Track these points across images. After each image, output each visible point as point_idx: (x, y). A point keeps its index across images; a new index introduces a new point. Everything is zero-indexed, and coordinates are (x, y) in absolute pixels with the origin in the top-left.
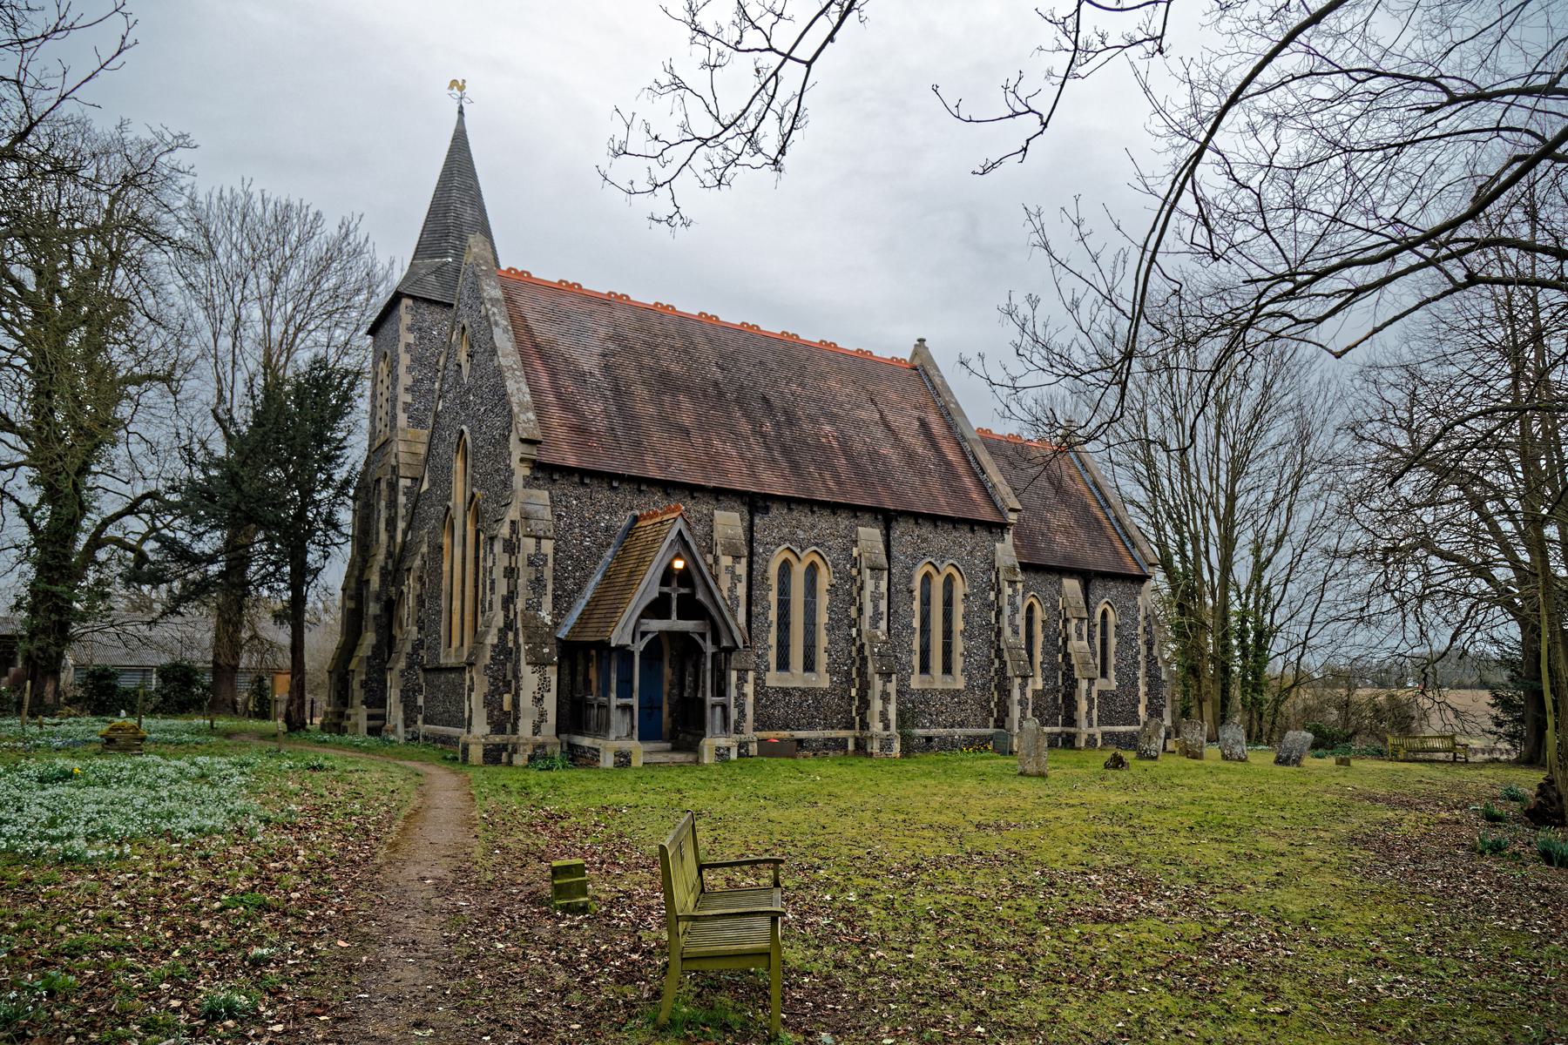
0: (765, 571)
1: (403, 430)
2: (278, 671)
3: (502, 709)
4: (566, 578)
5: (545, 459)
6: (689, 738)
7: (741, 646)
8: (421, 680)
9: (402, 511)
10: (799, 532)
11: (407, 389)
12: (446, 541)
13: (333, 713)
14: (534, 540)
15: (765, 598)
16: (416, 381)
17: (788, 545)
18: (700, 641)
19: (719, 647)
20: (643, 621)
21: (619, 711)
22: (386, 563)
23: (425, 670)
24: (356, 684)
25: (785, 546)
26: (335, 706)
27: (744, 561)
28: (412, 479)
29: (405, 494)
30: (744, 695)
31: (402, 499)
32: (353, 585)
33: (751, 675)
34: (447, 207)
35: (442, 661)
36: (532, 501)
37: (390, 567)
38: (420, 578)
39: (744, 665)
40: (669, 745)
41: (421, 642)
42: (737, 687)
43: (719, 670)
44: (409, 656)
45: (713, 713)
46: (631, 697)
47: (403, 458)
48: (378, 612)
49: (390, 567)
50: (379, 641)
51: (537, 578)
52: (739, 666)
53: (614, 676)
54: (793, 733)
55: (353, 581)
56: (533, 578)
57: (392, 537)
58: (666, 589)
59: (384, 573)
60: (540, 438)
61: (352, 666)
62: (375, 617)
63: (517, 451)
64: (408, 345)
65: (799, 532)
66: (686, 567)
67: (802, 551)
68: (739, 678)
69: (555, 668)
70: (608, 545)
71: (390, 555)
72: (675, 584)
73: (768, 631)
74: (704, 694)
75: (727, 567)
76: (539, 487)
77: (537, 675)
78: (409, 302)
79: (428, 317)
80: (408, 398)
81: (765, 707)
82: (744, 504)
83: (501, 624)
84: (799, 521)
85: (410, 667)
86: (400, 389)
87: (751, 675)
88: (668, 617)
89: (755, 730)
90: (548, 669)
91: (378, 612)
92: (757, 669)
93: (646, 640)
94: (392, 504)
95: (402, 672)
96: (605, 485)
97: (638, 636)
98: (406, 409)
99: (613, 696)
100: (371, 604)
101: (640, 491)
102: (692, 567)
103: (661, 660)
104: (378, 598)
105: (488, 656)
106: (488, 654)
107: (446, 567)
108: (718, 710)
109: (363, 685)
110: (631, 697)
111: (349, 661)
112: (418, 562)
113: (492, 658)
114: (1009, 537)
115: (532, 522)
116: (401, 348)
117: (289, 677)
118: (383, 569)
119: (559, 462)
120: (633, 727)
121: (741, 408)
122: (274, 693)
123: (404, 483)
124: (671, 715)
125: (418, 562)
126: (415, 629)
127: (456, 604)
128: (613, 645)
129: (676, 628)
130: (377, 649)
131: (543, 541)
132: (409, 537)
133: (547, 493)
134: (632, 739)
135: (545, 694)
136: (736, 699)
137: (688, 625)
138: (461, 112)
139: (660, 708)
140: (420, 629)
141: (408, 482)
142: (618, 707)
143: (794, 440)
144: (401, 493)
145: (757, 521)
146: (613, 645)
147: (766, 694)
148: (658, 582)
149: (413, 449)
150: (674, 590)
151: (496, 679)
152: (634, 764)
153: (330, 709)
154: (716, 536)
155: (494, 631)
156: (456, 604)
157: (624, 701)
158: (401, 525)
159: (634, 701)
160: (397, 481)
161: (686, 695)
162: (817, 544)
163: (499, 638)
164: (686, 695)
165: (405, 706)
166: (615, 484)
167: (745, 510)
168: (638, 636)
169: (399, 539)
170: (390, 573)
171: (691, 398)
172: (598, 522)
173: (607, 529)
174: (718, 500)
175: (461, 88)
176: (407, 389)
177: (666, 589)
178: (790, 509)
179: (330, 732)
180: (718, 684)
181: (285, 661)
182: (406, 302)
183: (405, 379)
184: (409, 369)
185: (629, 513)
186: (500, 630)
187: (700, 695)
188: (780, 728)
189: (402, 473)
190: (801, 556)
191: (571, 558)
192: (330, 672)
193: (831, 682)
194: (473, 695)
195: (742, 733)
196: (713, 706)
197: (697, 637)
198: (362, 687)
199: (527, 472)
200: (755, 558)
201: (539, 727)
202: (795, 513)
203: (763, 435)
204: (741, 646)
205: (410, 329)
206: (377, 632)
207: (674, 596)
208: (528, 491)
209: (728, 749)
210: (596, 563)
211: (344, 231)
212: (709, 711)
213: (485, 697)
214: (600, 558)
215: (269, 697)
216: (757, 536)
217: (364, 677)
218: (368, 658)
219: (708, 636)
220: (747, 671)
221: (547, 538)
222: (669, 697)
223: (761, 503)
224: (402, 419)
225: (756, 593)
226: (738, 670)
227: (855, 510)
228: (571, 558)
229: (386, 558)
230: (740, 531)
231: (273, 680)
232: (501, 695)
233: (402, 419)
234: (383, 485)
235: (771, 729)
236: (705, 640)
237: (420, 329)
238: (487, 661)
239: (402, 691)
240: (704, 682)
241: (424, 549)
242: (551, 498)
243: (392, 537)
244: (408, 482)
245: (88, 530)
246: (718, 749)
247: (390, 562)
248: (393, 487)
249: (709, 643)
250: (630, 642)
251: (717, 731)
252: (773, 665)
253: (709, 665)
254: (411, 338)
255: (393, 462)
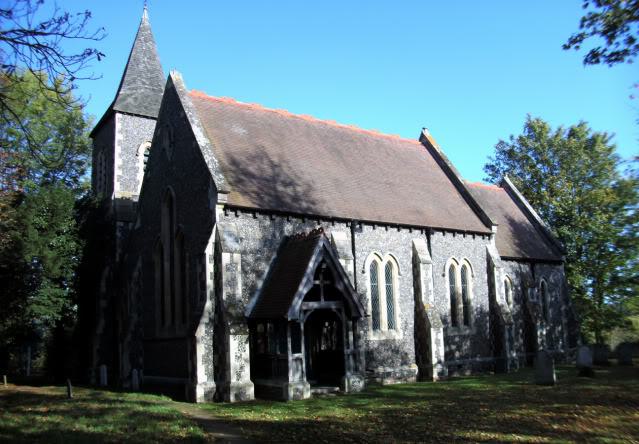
12: (156, 258)
53: (289, 340)
64: (120, 141)
79: (131, 124)
99: (290, 352)
107: (157, 275)
114: (493, 241)
127: (168, 298)
137: (333, 306)
140: (139, 315)
145: (356, 237)
156: (168, 298)
157: (296, 355)
159: (301, 355)
162: (390, 250)
179: (504, 419)
193: (404, 335)
227: (410, 228)
245: (569, 141)
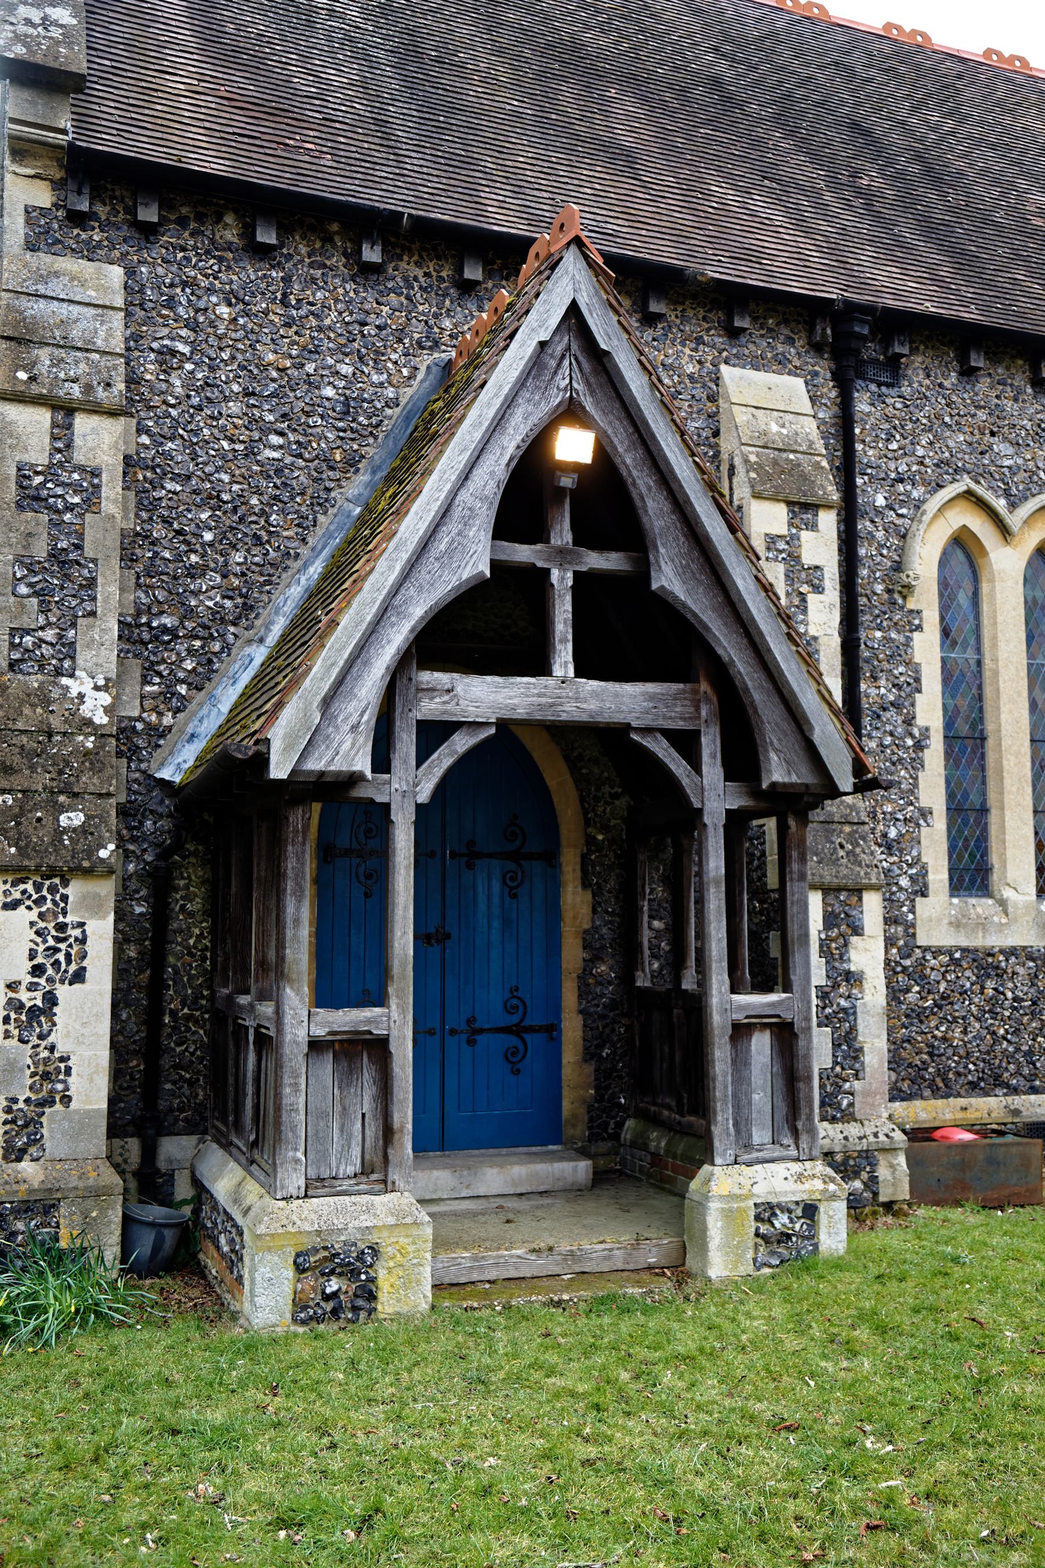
0: (898, 567)
4: (194, 573)
5: (107, 143)
6: (658, 1140)
7: (845, 781)
10: (1000, 447)
14: (43, 417)
15: (901, 653)
17: (965, 483)
18: (678, 766)
19: (756, 792)
20: (426, 677)
21: (326, 1067)
25: (959, 487)
27: (828, 521)
30: (853, 979)
33: (872, 906)
36: (55, 288)
39: (844, 872)
40: (581, 1169)
42: (825, 950)
43: (759, 892)
45: (740, 1062)
46: (381, 1001)
51: (54, 555)
52: (828, 875)
54: (1018, 1101)
56: (40, 550)
58: (523, 553)
60: (81, 66)
63: (813, 992)
65: (1000, 447)
66: (602, 452)
67: (1013, 506)
68: (830, 920)
69: (106, 889)
70: (352, 463)
72: (562, 534)
73: (917, 764)
74: (703, 982)
75: (771, 540)
76: (89, 252)
77: (24, 916)
81: (919, 1015)
82: (817, 348)
84: (997, 412)
87: (872, 906)
88: (541, 667)
89: (896, 1094)
90: (74, 890)
92: (887, 885)
93: (443, 760)
96: (336, 260)
97: (406, 744)
101: (467, 288)
102: (629, 460)
103: (551, 857)
108: (761, 1044)
110: (381, 1001)
115: (44, 355)
119: (159, 155)
120: (388, 1133)
121: (791, 134)
124: (590, 1053)
128: (279, 770)
129: (570, 711)
131: (82, 423)
133: (116, 273)
134: (386, 1186)
135: (63, 991)
136: (824, 995)
139: (552, 1031)
142: (315, 1046)
143: (952, 210)
145: (862, 405)
146: (279, 770)
147: (919, 974)
148: (485, 516)
150: (562, 555)
152: (386, 1305)
154: (727, 444)
161: (642, 981)
164: (642, 981)
166: (371, 254)
167: (823, 368)
168: (406, 744)
171: (645, 100)
172: (311, 384)
173: (347, 408)
174: (733, 334)
177: (523, 553)
178: (968, 373)
180: (758, 941)
185: (426, 360)
187: (688, 983)
188: (973, 1088)
190: (1015, 520)
191: (213, 501)
195: (848, 1116)
196: (740, 1032)
197: (661, 749)
199: (43, 196)
200: (863, 525)
201: (32, 1123)
202: (983, 385)
203: (868, 196)
204: (845, 781)
207: (561, 579)
208: (44, 260)
209: (810, 1211)
210: (305, 525)
212: (721, 1055)
214: (321, 504)
216: (866, 453)
219: (710, 745)
220: (857, 891)
221: (96, 409)
222: (584, 991)
223: (871, 351)
225: (872, 636)
226: (827, 891)
228: (213, 501)
230: (810, 427)
235: (941, 1088)
236: (695, 763)
240: (701, 935)
242: (133, 289)
246: (766, 1212)
249: (712, 770)
250: (363, 764)
251: (760, 1135)
252: (939, 876)
253: (715, 864)
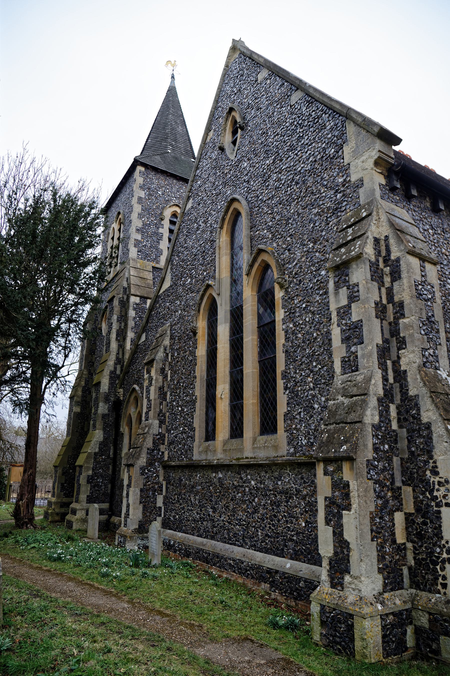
1: (134, 260)
2: (13, 464)
3: (394, 541)
8: (161, 479)
9: (131, 323)
11: (138, 230)
13: (56, 503)
16: (144, 224)
22: (115, 368)
23: (166, 467)
24: (83, 480)
26: (58, 497)
28: (141, 297)
29: (134, 309)
31: (132, 313)
32: (80, 393)
34: (166, 124)
35: (196, 457)
37: (118, 372)
38: (162, 371)
41: (162, 436)
44: (150, 452)
47: (133, 280)
48: (107, 412)
49: (118, 372)
50: (105, 439)
51: (428, 318)
55: (80, 389)
57: (121, 347)
59: (113, 376)
61: (81, 460)
62: (104, 416)
64: (140, 199)
71: (119, 361)
78: (143, 169)
80: (139, 237)
83: (381, 392)
85: (150, 463)
86: (133, 230)
91: (107, 412)
94: (123, 318)
95: (142, 469)
98: (137, 243)
100: (101, 404)
104: (107, 399)
105: (370, 446)
106: (370, 441)
109: (90, 480)
111: (76, 457)
112: (160, 355)
113: (376, 449)
116: (134, 201)
117: (21, 469)
118: (113, 373)
122: (9, 480)
123: (134, 300)
125: (160, 355)
126: (156, 422)
130: (103, 445)
132: (143, 338)
138: (173, 77)
140: (162, 422)
141: (137, 300)
144: (131, 308)
149: (141, 275)
151: (382, 485)
153: (54, 500)
155: (373, 402)
158: (130, 335)
160: (128, 298)
163: (381, 416)
165: (144, 507)
169: (128, 346)
170: (118, 377)
175: (174, 65)
176: (138, 230)
181: (21, 458)
182: (139, 168)
183: (137, 223)
184: (140, 216)
186: (379, 400)
189: (133, 291)
192: (55, 467)
194: (131, 489)
198: (88, 482)
205: (142, 187)
206: (104, 429)
211: (81, 184)
213: (372, 519)
215: (6, 482)
217: (90, 472)
218: (95, 453)
224: (133, 252)
229: (116, 364)
231: (10, 471)
232: (391, 513)
233: (133, 252)
234: (116, 302)
237: (149, 189)
238: (370, 454)
239: (141, 490)
241: (167, 342)
243: (121, 347)
244: (137, 300)
247: (119, 367)
248: (124, 304)
254: (142, 194)
255: (125, 284)
